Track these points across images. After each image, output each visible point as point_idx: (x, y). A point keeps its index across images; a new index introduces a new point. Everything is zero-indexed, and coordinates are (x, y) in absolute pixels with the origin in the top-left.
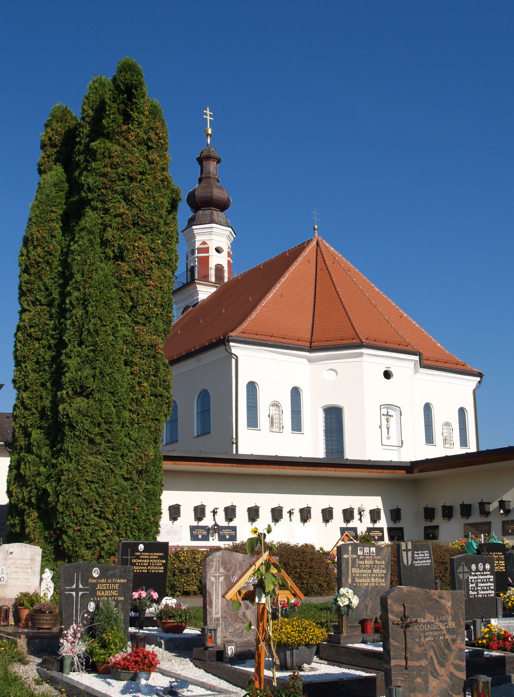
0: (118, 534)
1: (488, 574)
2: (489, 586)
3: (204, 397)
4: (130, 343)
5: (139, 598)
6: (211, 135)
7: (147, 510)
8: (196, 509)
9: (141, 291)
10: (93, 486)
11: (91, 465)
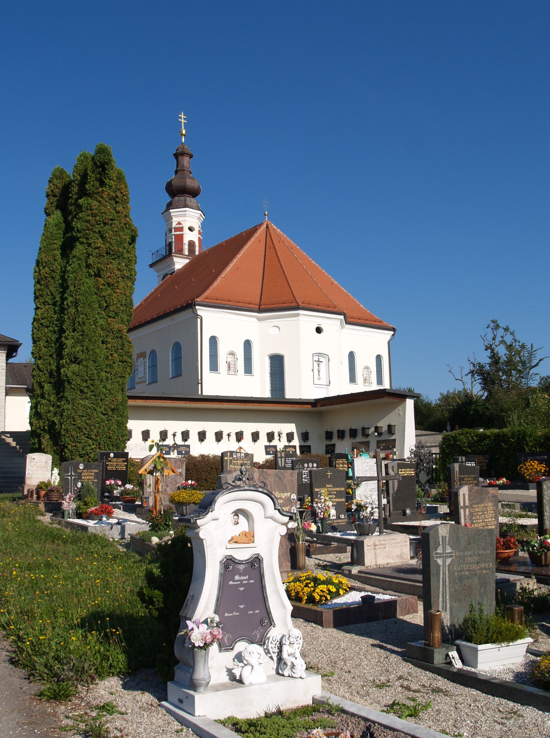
0: (100, 448)
3: (177, 347)
5: (110, 484)
6: (184, 135)
10: (83, 419)
11: (82, 406)
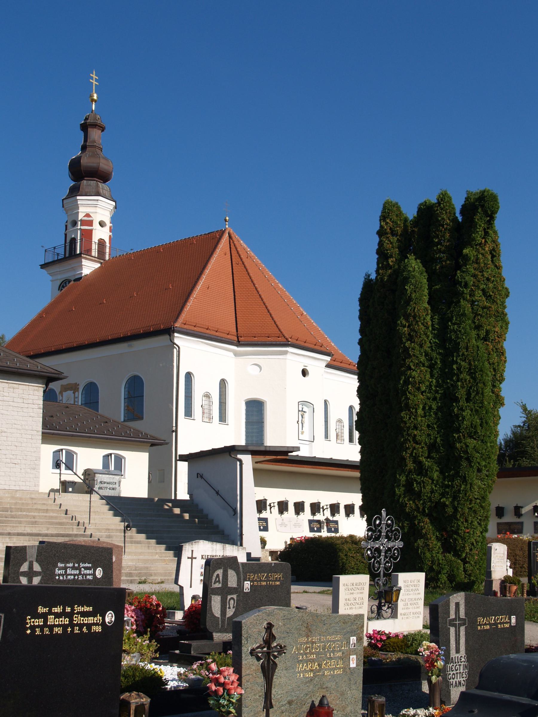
6: (96, 101)
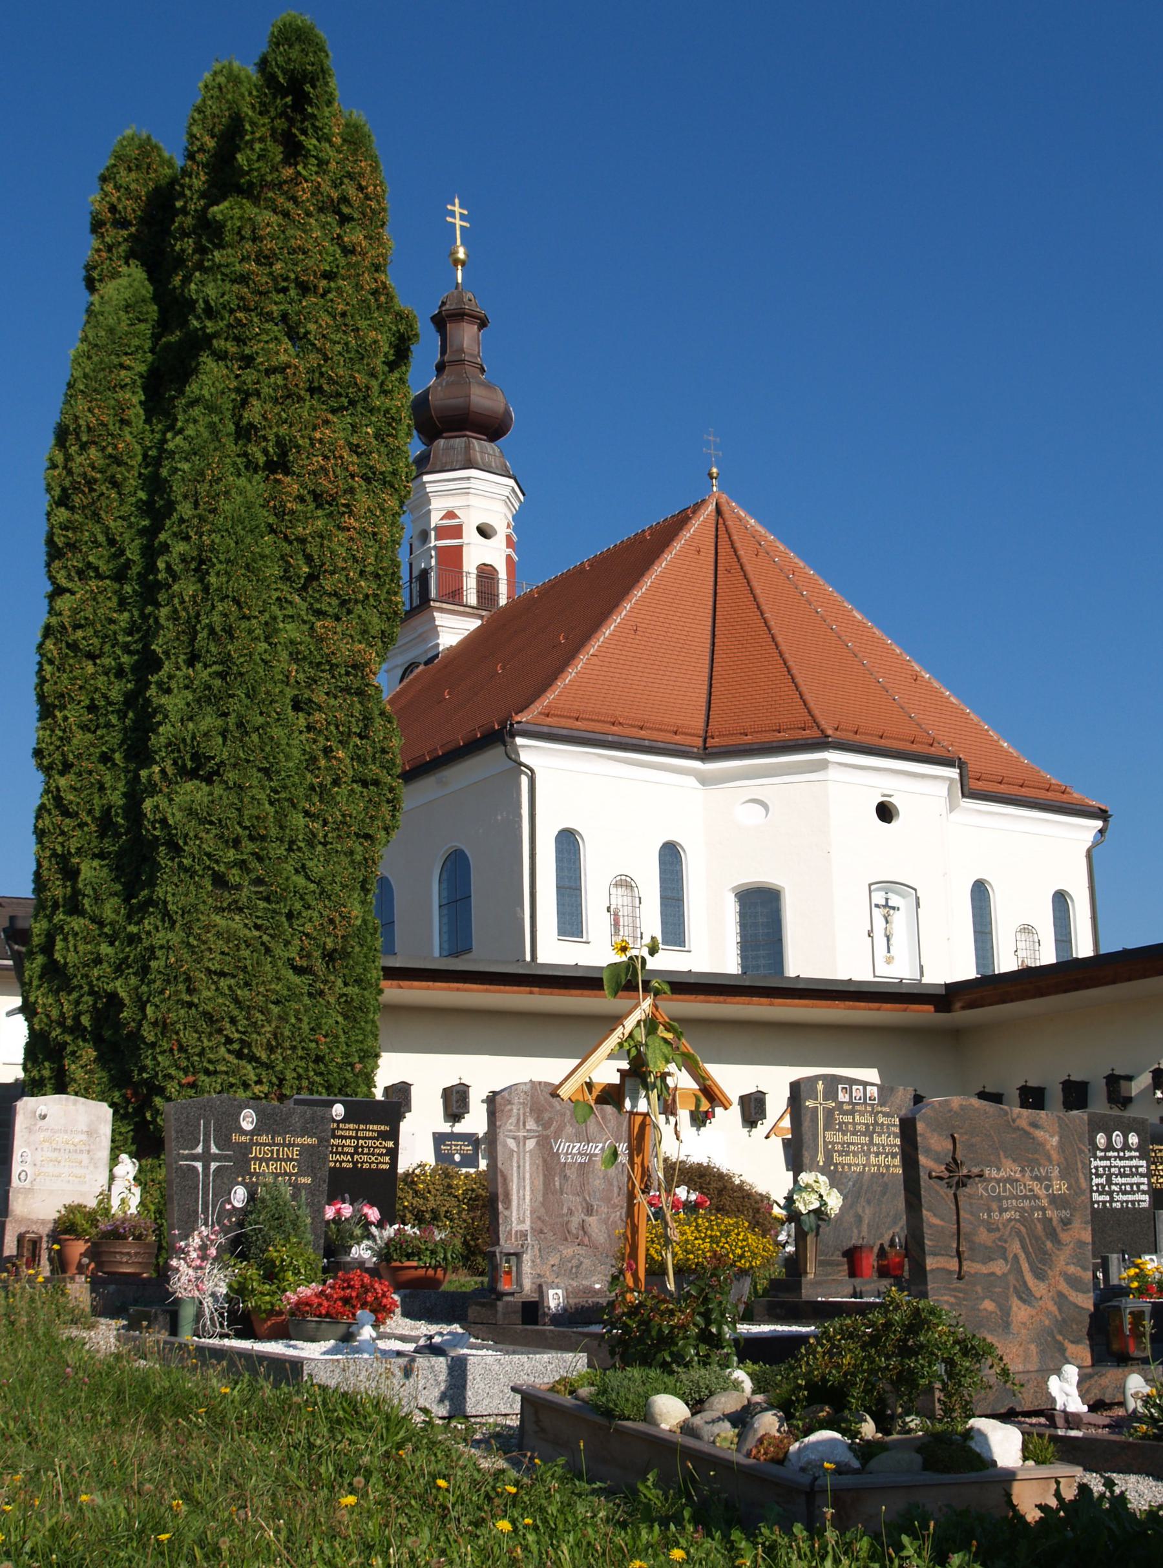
1: (1135, 1157)
2: (1138, 1185)
3: (457, 868)
4: (305, 658)
5: (337, 1221)
6: (463, 264)
7: (347, 1045)
8: (447, 1093)
9: (330, 541)
10: (224, 983)
11: (218, 935)
